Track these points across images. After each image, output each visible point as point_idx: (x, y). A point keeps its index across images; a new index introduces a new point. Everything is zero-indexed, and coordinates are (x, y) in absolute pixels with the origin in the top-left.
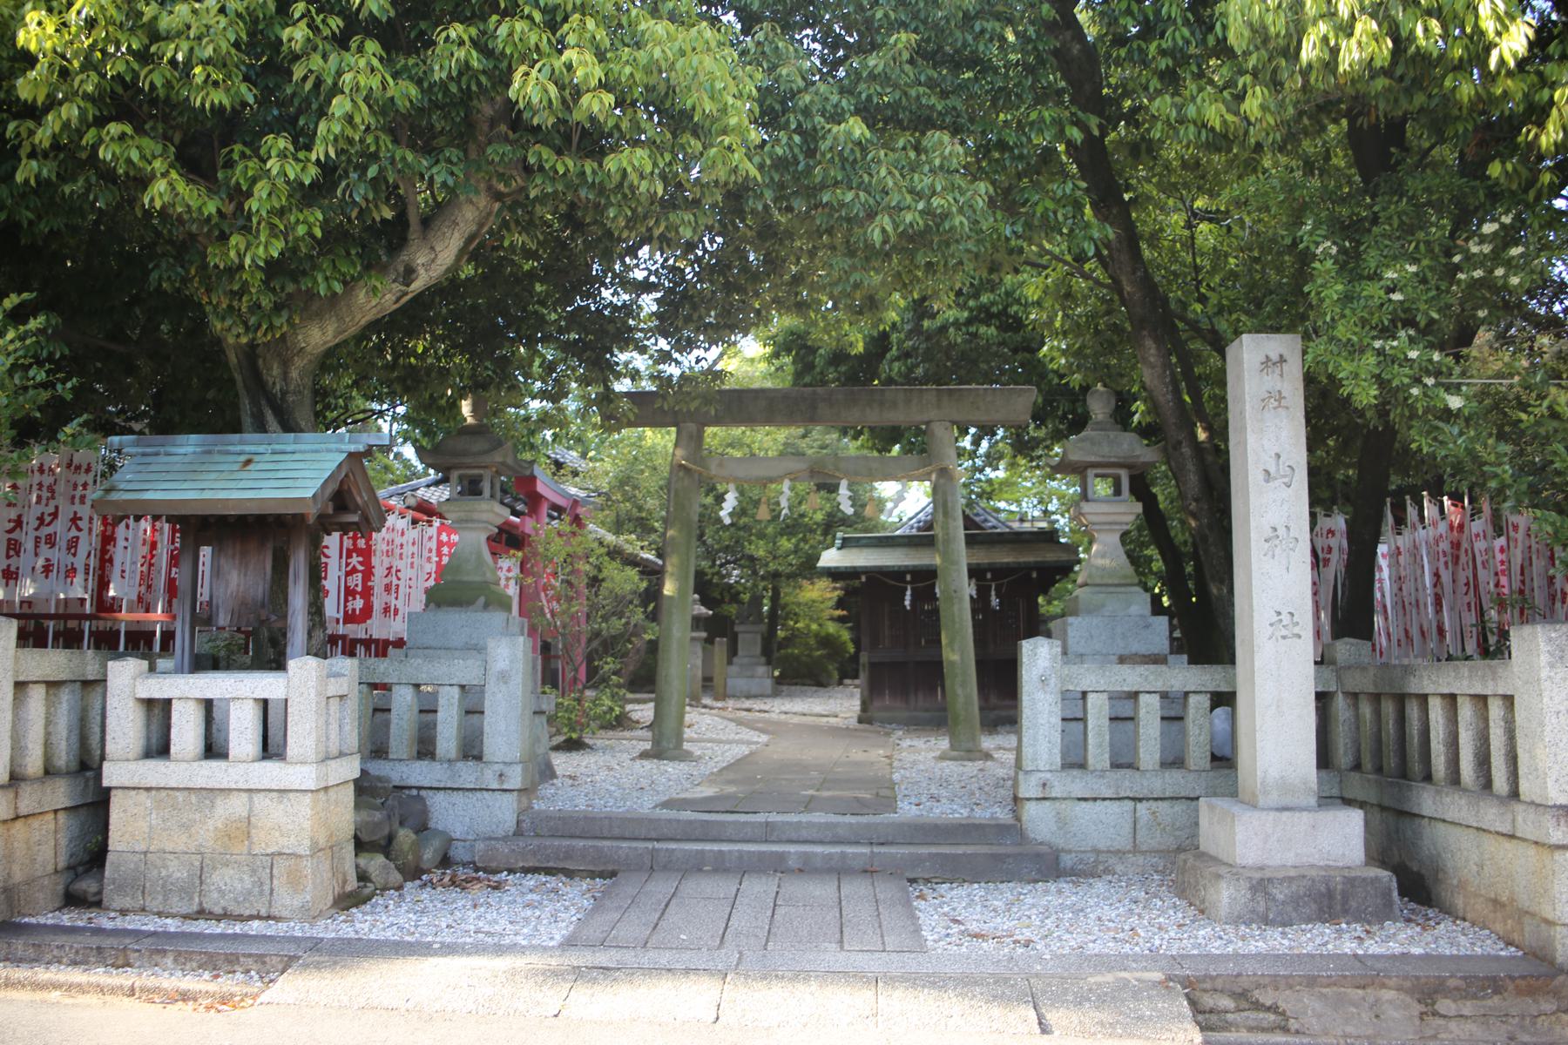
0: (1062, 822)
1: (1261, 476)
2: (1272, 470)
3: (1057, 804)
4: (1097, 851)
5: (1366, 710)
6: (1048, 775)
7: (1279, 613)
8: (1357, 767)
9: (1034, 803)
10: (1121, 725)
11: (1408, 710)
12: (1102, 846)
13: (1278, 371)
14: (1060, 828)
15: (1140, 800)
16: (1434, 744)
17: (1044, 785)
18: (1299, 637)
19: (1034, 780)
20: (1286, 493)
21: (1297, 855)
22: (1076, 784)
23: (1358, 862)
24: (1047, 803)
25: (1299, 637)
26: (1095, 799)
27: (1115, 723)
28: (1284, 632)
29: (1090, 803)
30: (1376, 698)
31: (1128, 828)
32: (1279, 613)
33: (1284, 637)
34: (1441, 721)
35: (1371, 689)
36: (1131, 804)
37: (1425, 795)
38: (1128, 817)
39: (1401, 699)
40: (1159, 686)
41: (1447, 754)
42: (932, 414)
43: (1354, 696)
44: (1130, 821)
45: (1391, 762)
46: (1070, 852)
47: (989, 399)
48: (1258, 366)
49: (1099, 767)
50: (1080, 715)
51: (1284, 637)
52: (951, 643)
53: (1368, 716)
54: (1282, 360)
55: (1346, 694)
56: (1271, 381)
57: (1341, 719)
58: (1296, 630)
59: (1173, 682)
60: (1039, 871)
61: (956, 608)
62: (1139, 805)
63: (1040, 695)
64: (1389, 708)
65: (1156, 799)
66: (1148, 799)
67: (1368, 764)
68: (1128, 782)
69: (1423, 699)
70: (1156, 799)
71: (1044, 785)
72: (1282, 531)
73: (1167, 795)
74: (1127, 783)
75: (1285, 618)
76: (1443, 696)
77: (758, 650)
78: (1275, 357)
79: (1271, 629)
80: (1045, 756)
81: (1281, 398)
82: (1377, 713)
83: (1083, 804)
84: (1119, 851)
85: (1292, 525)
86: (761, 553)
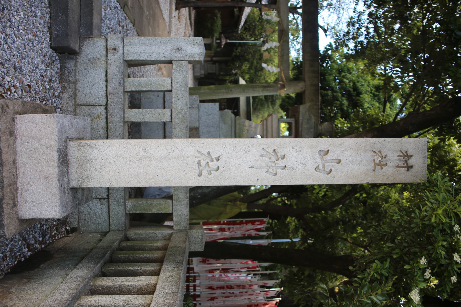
0: (93, 61)
1: (324, 148)
2: (328, 157)
3: (104, 59)
4: (76, 82)
5: (159, 244)
6: (121, 52)
7: (218, 159)
8: (127, 239)
9: (105, 44)
10: (161, 127)
11: (152, 264)
12: (79, 85)
13: (401, 164)
14: (89, 60)
15: (106, 109)
16: (123, 278)
17: (115, 49)
18: (200, 175)
19: (118, 43)
20: (311, 167)
21: (25, 164)
22: (115, 69)
23: (21, 213)
24: (104, 52)
25: (200, 175)
26: (106, 81)
27: (163, 124)
28: (203, 163)
29: (104, 78)
30: (165, 248)
31: (90, 100)
32: (218, 159)
33: (199, 163)
34: (138, 284)
35: (171, 245)
36: (104, 103)
37: (86, 271)
38: (96, 101)
39: (161, 261)
40: (175, 120)
41: (113, 287)
42: (308, 83)
43: (169, 238)
44: (94, 102)
45: (121, 255)
46: (75, 66)
47: (315, 107)
48: (405, 149)
49: (126, 84)
50: (162, 93)
51: (199, 163)
52: (210, 89)
53: (155, 245)
54: (409, 167)
55: (171, 235)
56: (393, 159)
57: (157, 232)
58: (205, 173)
59: (178, 129)
60: (57, 36)
61: (224, 91)
62: (103, 108)
63: (169, 47)
64: (157, 255)
65: (107, 118)
66: (106, 113)
67: (124, 244)
68: (118, 101)
69: (157, 273)
70: (107, 118)
71: (115, 49)
72: (281, 163)
73: (109, 125)
74: (116, 100)
75: (214, 165)
76: (155, 285)
77: (210, 71)
78: (411, 162)
79: (205, 152)
80: (132, 50)
81: (382, 165)
82: (158, 249)
83: (104, 74)
84: (76, 95)
85: (287, 170)
86: (244, 67)
